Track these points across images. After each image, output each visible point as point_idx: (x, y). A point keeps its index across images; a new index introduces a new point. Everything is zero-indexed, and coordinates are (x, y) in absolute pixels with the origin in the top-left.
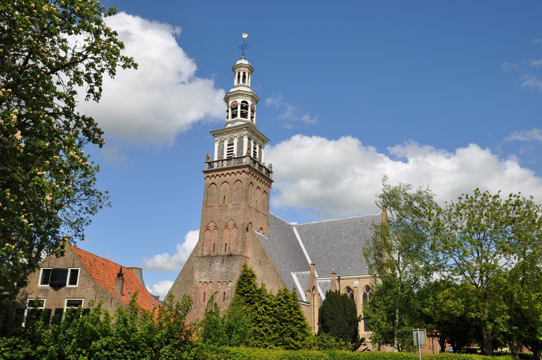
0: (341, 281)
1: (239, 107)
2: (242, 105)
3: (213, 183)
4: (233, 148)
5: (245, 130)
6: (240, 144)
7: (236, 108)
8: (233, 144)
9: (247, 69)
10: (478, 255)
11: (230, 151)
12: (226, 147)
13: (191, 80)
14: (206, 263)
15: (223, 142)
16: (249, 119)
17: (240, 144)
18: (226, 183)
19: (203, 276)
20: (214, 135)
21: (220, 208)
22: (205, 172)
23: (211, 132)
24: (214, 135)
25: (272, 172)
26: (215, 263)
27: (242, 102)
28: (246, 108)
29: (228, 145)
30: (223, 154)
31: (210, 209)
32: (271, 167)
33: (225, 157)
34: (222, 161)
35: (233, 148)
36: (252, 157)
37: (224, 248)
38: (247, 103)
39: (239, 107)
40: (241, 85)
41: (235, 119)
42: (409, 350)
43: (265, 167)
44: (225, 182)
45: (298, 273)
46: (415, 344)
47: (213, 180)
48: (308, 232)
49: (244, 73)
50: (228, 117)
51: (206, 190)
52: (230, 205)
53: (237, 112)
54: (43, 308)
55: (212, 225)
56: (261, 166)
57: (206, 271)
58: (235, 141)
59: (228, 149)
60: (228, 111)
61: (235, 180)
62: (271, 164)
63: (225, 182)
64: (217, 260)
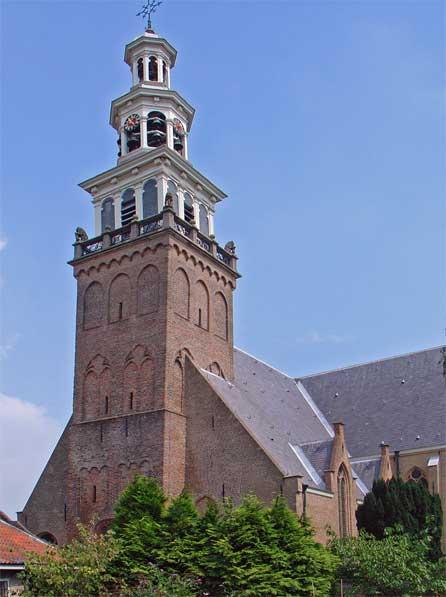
0: (400, 460)
1: (144, 126)
3: (94, 283)
4: (135, 213)
7: (138, 129)
8: (134, 200)
13: (134, 266)
14: (94, 434)
15: (112, 200)
18: (119, 280)
19: (88, 457)
21: (112, 327)
25: (236, 259)
26: (111, 432)
27: (151, 114)
28: (163, 127)
29: (124, 205)
31: (93, 332)
32: (233, 248)
33: (118, 225)
34: (113, 234)
36: (183, 218)
37: (127, 403)
38: (163, 117)
39: (144, 126)
41: (135, 153)
42: (356, 465)
44: (119, 275)
47: (95, 276)
49: (153, 59)
52: (134, 319)
53: (139, 137)
55: (98, 365)
56: (209, 242)
57: (93, 447)
58: (139, 195)
60: (119, 142)
61: (141, 268)
62: (232, 243)
63: (119, 275)
64: (114, 425)
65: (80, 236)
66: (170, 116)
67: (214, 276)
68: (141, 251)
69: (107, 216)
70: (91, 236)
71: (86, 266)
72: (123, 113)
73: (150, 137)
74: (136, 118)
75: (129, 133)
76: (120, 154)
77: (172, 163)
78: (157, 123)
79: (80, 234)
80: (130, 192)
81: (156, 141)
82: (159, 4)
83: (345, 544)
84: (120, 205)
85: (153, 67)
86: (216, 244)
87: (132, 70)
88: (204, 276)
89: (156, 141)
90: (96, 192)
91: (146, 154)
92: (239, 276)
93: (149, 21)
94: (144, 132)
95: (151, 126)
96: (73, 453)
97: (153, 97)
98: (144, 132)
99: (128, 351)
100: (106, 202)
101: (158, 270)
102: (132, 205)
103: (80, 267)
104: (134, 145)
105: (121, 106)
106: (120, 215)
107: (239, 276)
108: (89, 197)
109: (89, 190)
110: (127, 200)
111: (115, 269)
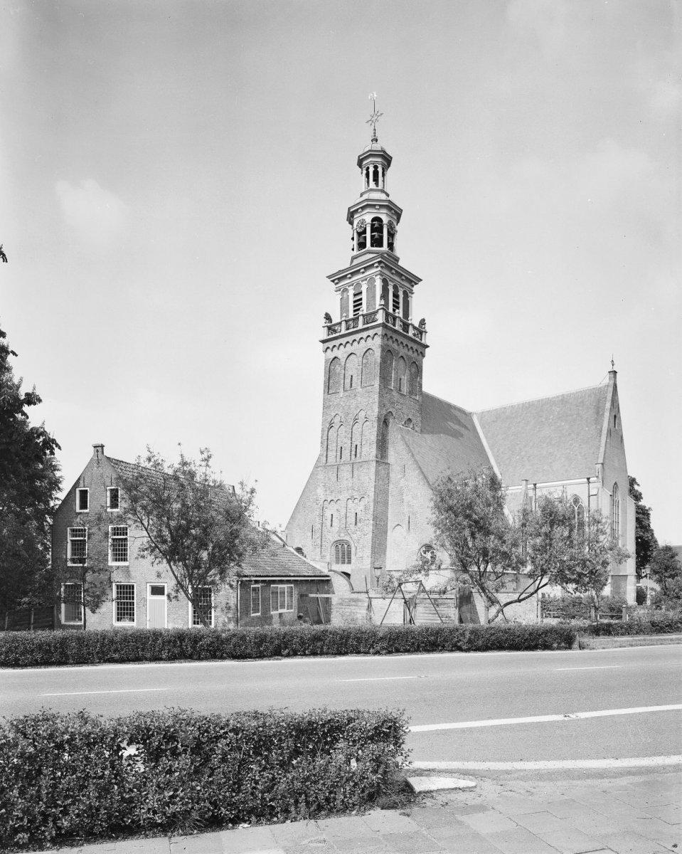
2: (372, 225)
5: (377, 267)
6: (371, 289)
7: (364, 232)
8: (355, 311)
9: (379, 160)
10: (479, 568)
11: (358, 304)
12: (351, 299)
16: (385, 248)
17: (371, 289)
20: (333, 281)
22: (323, 342)
23: (329, 277)
24: (333, 281)
27: (374, 219)
28: (380, 230)
29: (355, 295)
30: (347, 311)
33: (351, 316)
35: (361, 299)
40: (372, 190)
43: (413, 325)
45: (319, 628)
46: (540, 603)
47: (336, 353)
48: (482, 415)
49: (376, 167)
50: (353, 249)
51: (328, 369)
53: (365, 237)
54: (111, 563)
58: (364, 288)
59: (355, 302)
60: (353, 239)
66: (385, 219)
67: (411, 350)
69: (344, 308)
71: (330, 344)
73: (372, 237)
74: (363, 221)
75: (359, 234)
77: (396, 271)
79: (328, 317)
80: (359, 285)
81: (377, 242)
82: (381, 114)
85: (376, 173)
87: (362, 173)
88: (403, 351)
89: (377, 242)
90: (337, 283)
91: (370, 252)
92: (427, 346)
94: (368, 235)
96: (319, 489)
97: (392, 209)
98: (368, 235)
99: (356, 413)
100: (343, 291)
103: (327, 344)
105: (354, 211)
106: (340, 565)
107: (427, 346)
111: (349, 349)
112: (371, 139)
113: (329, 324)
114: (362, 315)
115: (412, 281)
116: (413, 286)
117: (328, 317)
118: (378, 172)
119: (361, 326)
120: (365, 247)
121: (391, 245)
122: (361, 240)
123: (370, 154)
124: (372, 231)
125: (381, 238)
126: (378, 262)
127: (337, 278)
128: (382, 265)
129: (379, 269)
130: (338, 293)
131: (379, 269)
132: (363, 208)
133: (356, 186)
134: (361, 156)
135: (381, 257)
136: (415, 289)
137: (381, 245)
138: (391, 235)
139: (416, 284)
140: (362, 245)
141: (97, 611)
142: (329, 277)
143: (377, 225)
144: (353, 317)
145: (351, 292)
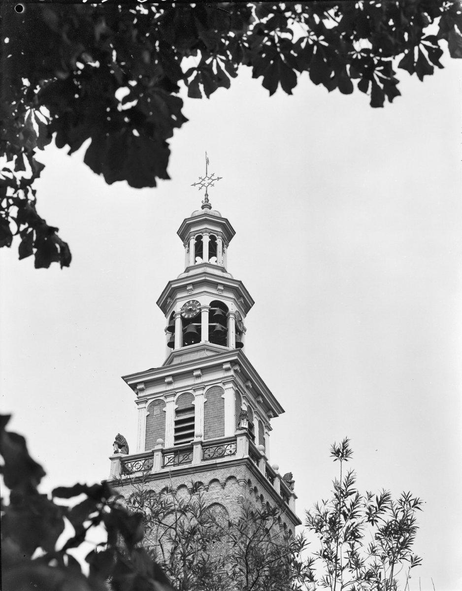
1: (205, 317)
2: (211, 313)
5: (228, 370)
7: (198, 318)
9: (219, 230)
11: (184, 427)
15: (163, 404)
23: (126, 379)
25: (296, 498)
27: (214, 304)
39: (205, 317)
49: (199, 239)
53: (199, 329)
58: (199, 402)
59: (177, 423)
65: (120, 447)
66: (232, 307)
68: (222, 480)
69: (153, 429)
70: (133, 452)
72: (179, 296)
73: (211, 329)
76: (171, 345)
78: (219, 313)
79: (121, 443)
80: (187, 396)
81: (218, 337)
83: (353, 557)
84: (173, 413)
86: (266, 459)
87: (188, 251)
89: (218, 337)
90: (142, 390)
91: (204, 348)
93: (207, 195)
95: (185, 322)
100: (153, 405)
101: (227, 513)
102: (192, 423)
104: (191, 337)
108: (132, 395)
109: (133, 387)
110: (182, 407)
112: (202, 204)
113: (124, 455)
114: (201, 443)
115: (270, 409)
116: (270, 417)
117: (121, 443)
118: (216, 245)
119: (157, 469)
120: (198, 340)
121: (239, 345)
122: (191, 328)
123: (206, 220)
124: (211, 320)
125: (225, 333)
126: (231, 362)
127: (138, 383)
128: (237, 368)
129: (232, 373)
130: (143, 405)
131: (232, 373)
132: (195, 285)
133: (176, 261)
134: (189, 219)
135: (238, 355)
136: (273, 422)
137: (224, 342)
138: (239, 332)
139: (276, 416)
140: (191, 337)
141: (293, 90)
142: (126, 379)
143: (219, 313)
144: (172, 446)
145: (170, 408)
